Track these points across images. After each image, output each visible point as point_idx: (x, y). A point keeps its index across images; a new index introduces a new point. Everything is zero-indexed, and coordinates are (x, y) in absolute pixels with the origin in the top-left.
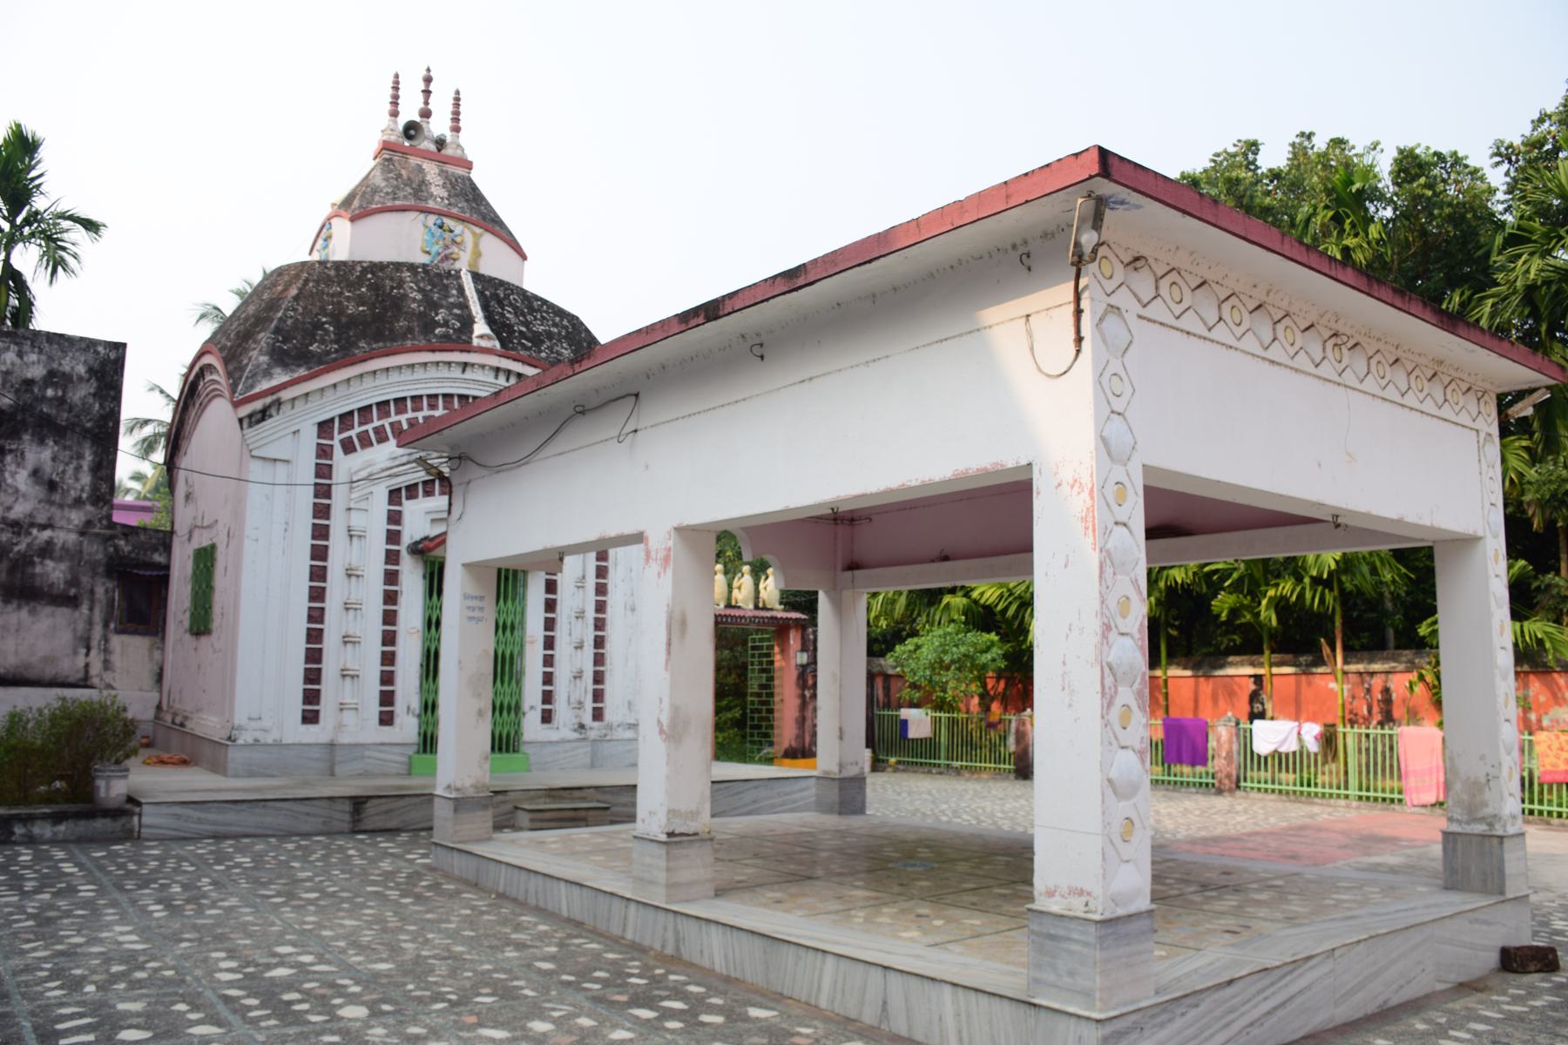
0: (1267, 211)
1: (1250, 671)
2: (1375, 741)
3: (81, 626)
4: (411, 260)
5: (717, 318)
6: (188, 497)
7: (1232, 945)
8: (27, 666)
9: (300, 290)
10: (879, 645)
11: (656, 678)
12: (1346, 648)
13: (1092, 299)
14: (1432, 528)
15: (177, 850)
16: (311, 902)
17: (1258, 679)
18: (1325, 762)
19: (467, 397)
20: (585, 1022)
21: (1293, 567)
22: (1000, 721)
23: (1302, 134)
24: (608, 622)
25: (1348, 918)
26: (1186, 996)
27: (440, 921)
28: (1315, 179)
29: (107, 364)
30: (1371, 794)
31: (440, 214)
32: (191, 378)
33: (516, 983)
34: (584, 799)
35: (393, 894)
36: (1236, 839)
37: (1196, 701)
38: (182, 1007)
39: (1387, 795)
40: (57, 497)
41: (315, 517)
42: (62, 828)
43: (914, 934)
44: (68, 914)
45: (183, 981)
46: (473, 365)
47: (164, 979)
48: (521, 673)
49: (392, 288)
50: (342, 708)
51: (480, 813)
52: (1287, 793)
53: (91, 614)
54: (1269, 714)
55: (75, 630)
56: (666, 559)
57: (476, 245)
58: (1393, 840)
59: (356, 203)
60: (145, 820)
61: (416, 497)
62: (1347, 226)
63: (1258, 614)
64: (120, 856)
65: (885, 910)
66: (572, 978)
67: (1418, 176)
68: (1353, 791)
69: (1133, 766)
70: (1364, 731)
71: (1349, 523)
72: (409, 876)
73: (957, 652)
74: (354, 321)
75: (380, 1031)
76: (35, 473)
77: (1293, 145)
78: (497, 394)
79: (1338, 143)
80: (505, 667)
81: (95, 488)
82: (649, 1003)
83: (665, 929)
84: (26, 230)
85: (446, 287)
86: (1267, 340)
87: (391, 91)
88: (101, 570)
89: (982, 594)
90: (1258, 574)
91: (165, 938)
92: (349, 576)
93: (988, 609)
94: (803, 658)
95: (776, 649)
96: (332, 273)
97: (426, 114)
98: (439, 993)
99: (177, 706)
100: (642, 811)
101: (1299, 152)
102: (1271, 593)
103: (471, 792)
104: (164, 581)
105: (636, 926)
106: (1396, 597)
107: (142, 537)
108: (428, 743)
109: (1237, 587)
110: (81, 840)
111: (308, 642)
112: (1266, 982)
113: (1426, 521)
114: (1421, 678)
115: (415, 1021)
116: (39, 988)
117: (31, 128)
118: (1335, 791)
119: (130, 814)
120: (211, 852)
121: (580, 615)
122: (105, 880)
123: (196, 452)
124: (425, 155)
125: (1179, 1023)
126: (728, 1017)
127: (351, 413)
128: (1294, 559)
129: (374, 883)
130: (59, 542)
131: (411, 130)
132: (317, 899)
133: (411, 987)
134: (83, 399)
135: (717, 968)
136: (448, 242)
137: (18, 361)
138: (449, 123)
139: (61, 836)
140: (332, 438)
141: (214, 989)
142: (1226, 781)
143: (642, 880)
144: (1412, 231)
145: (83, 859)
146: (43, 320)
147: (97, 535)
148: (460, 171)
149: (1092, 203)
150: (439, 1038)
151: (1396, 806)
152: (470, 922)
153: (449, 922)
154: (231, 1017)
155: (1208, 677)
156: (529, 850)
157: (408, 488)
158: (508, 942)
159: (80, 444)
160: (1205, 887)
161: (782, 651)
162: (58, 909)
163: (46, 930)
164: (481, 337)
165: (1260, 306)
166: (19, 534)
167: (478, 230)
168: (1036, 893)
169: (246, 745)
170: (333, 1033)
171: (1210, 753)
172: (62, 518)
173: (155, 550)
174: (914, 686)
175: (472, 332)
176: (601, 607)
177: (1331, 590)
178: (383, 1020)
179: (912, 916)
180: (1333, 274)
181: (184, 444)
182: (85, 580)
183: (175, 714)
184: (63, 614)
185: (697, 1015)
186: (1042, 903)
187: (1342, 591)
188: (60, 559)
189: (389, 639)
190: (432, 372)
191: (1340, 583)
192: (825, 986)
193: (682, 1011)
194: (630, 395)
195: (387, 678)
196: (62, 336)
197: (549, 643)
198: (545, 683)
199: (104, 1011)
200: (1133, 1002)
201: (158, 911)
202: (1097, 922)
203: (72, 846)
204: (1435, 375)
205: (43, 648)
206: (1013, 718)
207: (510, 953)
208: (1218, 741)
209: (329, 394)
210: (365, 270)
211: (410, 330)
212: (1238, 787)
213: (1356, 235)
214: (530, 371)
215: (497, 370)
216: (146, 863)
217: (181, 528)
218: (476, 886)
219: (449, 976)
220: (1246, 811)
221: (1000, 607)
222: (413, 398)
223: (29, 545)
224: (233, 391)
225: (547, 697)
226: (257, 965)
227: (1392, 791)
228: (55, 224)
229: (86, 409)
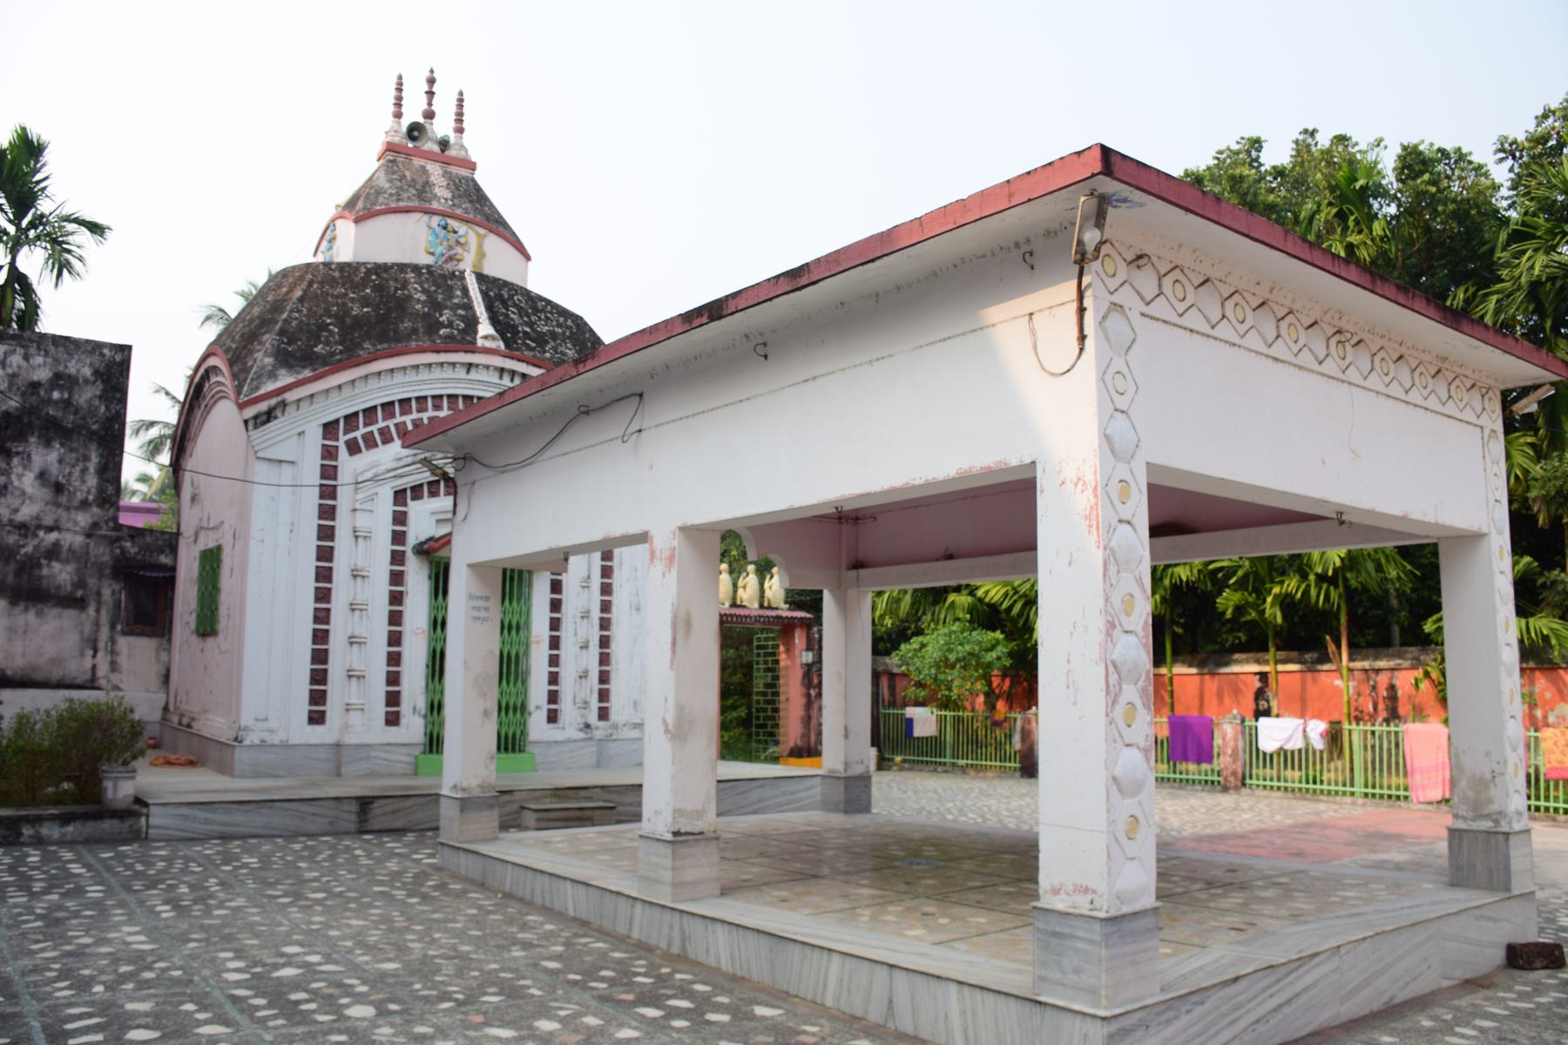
0: (1271, 208)
1: (1255, 668)
2: (1381, 738)
3: (88, 628)
4: (415, 261)
5: (720, 317)
6: (194, 499)
7: (1239, 943)
8: (35, 668)
9: (305, 291)
10: (884, 644)
11: (662, 678)
12: (1351, 645)
13: (1095, 297)
14: (1437, 525)
15: (184, 850)
16: (318, 902)
17: (1263, 676)
18: (1330, 760)
19: (471, 397)
20: (591, 1021)
21: (1299, 565)
22: (1006, 719)
23: (1306, 131)
24: (614, 622)
26: (1192, 993)
27: (446, 921)
28: (1319, 176)
29: (113, 366)
30: (1377, 791)
31: (444, 214)
32: (197, 379)
33: (522, 982)
34: (589, 799)
35: (400, 894)
37: (1201, 698)
38: (190, 1007)
39: (1393, 792)
40: (63, 499)
41: (320, 518)
42: (70, 829)
43: (919, 932)
44: (76, 915)
45: (191, 981)
46: (477, 366)
47: (171, 979)
48: (527, 673)
49: (397, 289)
50: (348, 708)
52: (1293, 790)
53: (95, 616)
54: (1275, 711)
55: (81, 632)
56: (671, 559)
57: (480, 246)
58: (1398, 838)
59: (360, 205)
60: (152, 821)
61: (421, 497)
62: (1351, 223)
63: (1263, 611)
64: (128, 857)
66: (578, 977)
67: (1422, 173)
68: (1359, 789)
69: (1137, 763)
70: (1369, 728)
72: (416, 876)
73: (962, 650)
74: (358, 322)
75: (387, 1030)
76: (42, 476)
77: (1296, 142)
78: (501, 394)
79: (1341, 139)
80: (511, 667)
81: (101, 490)
82: (655, 1002)
83: (671, 927)
84: (32, 233)
85: (450, 288)
87: (394, 93)
88: (107, 571)
89: (987, 593)
90: (1263, 572)
91: (172, 938)
92: (355, 577)
93: (993, 607)
94: (808, 657)
95: (782, 648)
96: (337, 274)
97: (429, 115)
99: (184, 707)
100: (647, 811)
102: (1276, 590)
103: (477, 792)
105: (642, 926)
106: (1401, 595)
107: (149, 539)
108: (434, 743)
109: (1241, 585)
110: (88, 841)
111: (314, 642)
112: (1273, 979)
113: (1430, 518)
114: (1427, 674)
115: (422, 1021)
116: (48, 989)
117: (36, 131)
118: (1340, 788)
119: (137, 815)
120: (219, 853)
121: (586, 615)
122: (113, 880)
124: (429, 156)
126: (734, 1016)
127: (356, 414)
128: (1299, 555)
129: (381, 883)
130: (66, 546)
131: (415, 131)
132: (324, 899)
133: (418, 986)
134: (89, 401)
135: (724, 968)
136: (452, 243)
137: (24, 364)
138: (452, 124)
139: (69, 837)
140: (337, 439)
141: (221, 989)
142: (1232, 779)
144: (1416, 228)
145: (92, 860)
146: (48, 324)
147: (104, 537)
148: (464, 172)
149: (1094, 201)
151: (1402, 803)
152: (477, 922)
155: (1213, 674)
156: (536, 850)
157: (413, 488)
158: (515, 942)
160: (1210, 884)
161: (788, 651)
164: (486, 337)
165: (1263, 304)
167: (482, 231)
168: (1041, 891)
169: (252, 746)
170: (340, 1032)
171: (1216, 750)
173: (162, 551)
174: (919, 685)
175: (476, 332)
176: (606, 607)
177: (1336, 587)
178: (390, 1019)
179: (918, 915)
180: (1336, 271)
181: (189, 446)
182: (92, 582)
183: (182, 715)
184: (69, 616)
185: (704, 1014)
186: (1046, 901)
187: (1347, 587)
188: (67, 561)
189: (395, 639)
190: (437, 373)
191: (1345, 580)
192: (832, 985)
193: (688, 1010)
194: (634, 395)
195: (393, 679)
196: (67, 338)
197: (555, 643)
198: (550, 683)
199: (113, 1011)
200: (1138, 1000)
201: (166, 912)
202: (1102, 920)
203: (79, 847)
205: (50, 650)
206: (1019, 716)
207: (517, 953)
209: (334, 395)
210: (369, 272)
211: (414, 331)
212: (1244, 785)
213: (1360, 232)
214: (534, 372)
215: (502, 371)
216: (154, 864)
217: (187, 529)
218: (482, 885)
219: (456, 976)
220: (1251, 808)
221: (1005, 606)
222: (418, 399)
223: (36, 547)
225: (553, 697)
226: (264, 965)
227: (1398, 788)
228: (61, 227)
229: (92, 412)
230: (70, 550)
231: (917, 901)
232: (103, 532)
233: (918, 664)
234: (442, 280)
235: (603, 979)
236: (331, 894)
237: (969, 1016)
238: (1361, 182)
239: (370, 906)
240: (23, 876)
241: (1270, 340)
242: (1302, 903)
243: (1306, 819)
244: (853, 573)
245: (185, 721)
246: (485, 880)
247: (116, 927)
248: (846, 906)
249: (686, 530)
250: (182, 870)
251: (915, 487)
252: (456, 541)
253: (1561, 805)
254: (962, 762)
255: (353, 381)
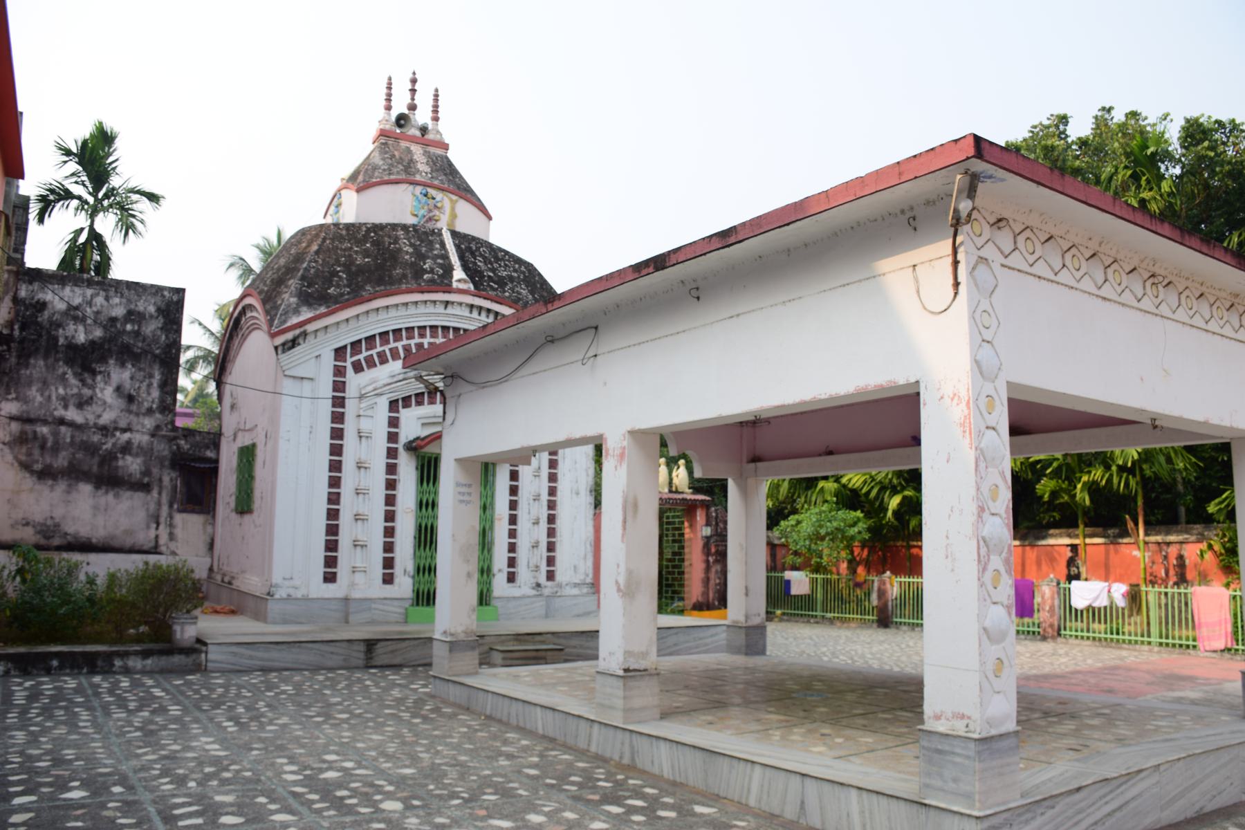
0: (1077, 172)
1: (1067, 541)
3: (152, 507)
4: (403, 222)
6: (233, 407)
8: (113, 537)
9: (320, 246)
10: (775, 517)
11: (606, 551)
12: (1147, 524)
13: (967, 252)
14: (1231, 428)
17: (1074, 548)
18: (1130, 616)
19: (459, 329)
20: (569, 815)
21: (1105, 460)
22: (865, 581)
23: (1103, 109)
24: (558, 503)
25: (1167, 740)
26: (1045, 799)
27: (445, 737)
28: (1116, 145)
29: (171, 305)
30: (1170, 641)
31: (425, 185)
32: (236, 314)
33: (511, 785)
34: (543, 642)
35: (406, 716)
36: (1062, 676)
38: (262, 800)
39: (1184, 642)
40: (134, 408)
42: (149, 662)
44: (164, 728)
45: (259, 780)
47: (244, 778)
49: (390, 244)
50: (354, 570)
51: (469, 653)
52: (1100, 639)
53: (160, 497)
54: (1084, 575)
55: (147, 510)
56: (622, 456)
57: (453, 209)
59: (361, 178)
60: (210, 656)
62: (1143, 183)
63: (1075, 495)
64: (194, 684)
65: (795, 730)
66: (554, 782)
67: (1202, 141)
69: (1002, 616)
70: (1163, 590)
71: (1165, 425)
72: (415, 702)
73: (831, 526)
74: (361, 270)
75: (414, 820)
76: (118, 389)
77: (1096, 118)
78: (484, 327)
79: (1134, 115)
81: (162, 401)
82: (617, 801)
83: (623, 744)
84: (106, 203)
85: (431, 242)
86: (1100, 282)
87: (385, 91)
88: (167, 463)
89: (850, 480)
91: (239, 747)
92: (359, 468)
93: (855, 492)
94: (707, 531)
95: (686, 524)
96: (344, 232)
97: (413, 107)
98: (454, 792)
99: (225, 568)
100: (602, 653)
101: (1101, 123)
103: (462, 637)
104: (214, 471)
105: (598, 742)
106: (1186, 482)
107: (198, 438)
108: (425, 597)
109: (1056, 474)
110: (162, 671)
111: (328, 519)
113: (1226, 423)
114: (1210, 547)
115: (440, 814)
116: (155, 783)
117: (109, 126)
118: (1139, 638)
120: (262, 682)
121: (537, 498)
122: (186, 702)
123: (239, 371)
125: (1039, 821)
126: (679, 813)
127: (360, 341)
129: (389, 707)
131: (402, 120)
132: (348, 719)
133: (431, 787)
134: (153, 332)
135: (666, 775)
136: (431, 207)
137: (105, 303)
138: (430, 114)
139: (148, 668)
141: (284, 787)
142: (1050, 630)
143: (602, 705)
145: (168, 687)
146: (118, 272)
147: (164, 436)
148: (439, 152)
149: (968, 178)
150: (460, 826)
151: (1191, 651)
153: (451, 737)
154: (300, 808)
155: (1032, 546)
157: (404, 399)
158: (501, 754)
159: (151, 366)
160: (1046, 714)
161: (691, 526)
162: (156, 723)
163: (152, 739)
164: (459, 281)
165: (1094, 255)
166: (106, 436)
167: (454, 198)
168: (925, 717)
169: (282, 599)
170: (379, 821)
171: (1036, 607)
172: (138, 423)
173: (207, 447)
174: (796, 553)
175: (451, 277)
176: (552, 492)
177: (1134, 476)
178: (415, 812)
179: (818, 735)
180: (1153, 228)
181: (229, 366)
182: (155, 471)
183: (224, 575)
184: (139, 497)
186: (930, 724)
188: (137, 455)
189: (390, 517)
190: (422, 309)
191: (1141, 470)
193: (643, 808)
194: (591, 328)
195: (389, 547)
197: (513, 520)
199: (206, 801)
201: (231, 727)
202: (976, 740)
203: (157, 676)
204: (1232, 305)
205: (125, 523)
206: (876, 579)
207: (503, 762)
208: (1043, 597)
209: (343, 327)
211: (404, 276)
212: (1059, 635)
213: (1151, 190)
214: (506, 311)
215: (472, 307)
216: (214, 690)
217: (228, 430)
218: (468, 710)
220: (1067, 654)
221: (864, 491)
222: (407, 329)
223: (114, 445)
224: (271, 325)
225: (512, 562)
226: (312, 769)
227: (1187, 639)
228: (127, 197)
229: (155, 340)
230: (139, 446)
231: (815, 725)
232: (163, 433)
233: (795, 537)
234: (425, 236)
235: (573, 783)
236: (353, 716)
237: (867, 815)
238: (1152, 149)
239: (384, 724)
240: (119, 697)
241: (1100, 283)
242: (1123, 731)
243: (1112, 663)
244: (752, 465)
245: (226, 579)
246: (470, 705)
247: (196, 737)
248: (760, 728)
249: (633, 433)
250: (236, 695)
251: (821, 400)
252: (446, 440)
253: (1240, 647)
254: (829, 615)
255: (358, 316)
